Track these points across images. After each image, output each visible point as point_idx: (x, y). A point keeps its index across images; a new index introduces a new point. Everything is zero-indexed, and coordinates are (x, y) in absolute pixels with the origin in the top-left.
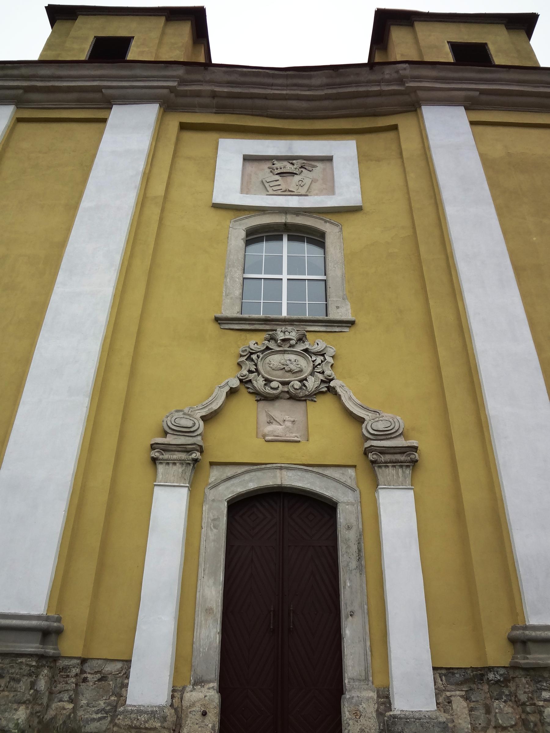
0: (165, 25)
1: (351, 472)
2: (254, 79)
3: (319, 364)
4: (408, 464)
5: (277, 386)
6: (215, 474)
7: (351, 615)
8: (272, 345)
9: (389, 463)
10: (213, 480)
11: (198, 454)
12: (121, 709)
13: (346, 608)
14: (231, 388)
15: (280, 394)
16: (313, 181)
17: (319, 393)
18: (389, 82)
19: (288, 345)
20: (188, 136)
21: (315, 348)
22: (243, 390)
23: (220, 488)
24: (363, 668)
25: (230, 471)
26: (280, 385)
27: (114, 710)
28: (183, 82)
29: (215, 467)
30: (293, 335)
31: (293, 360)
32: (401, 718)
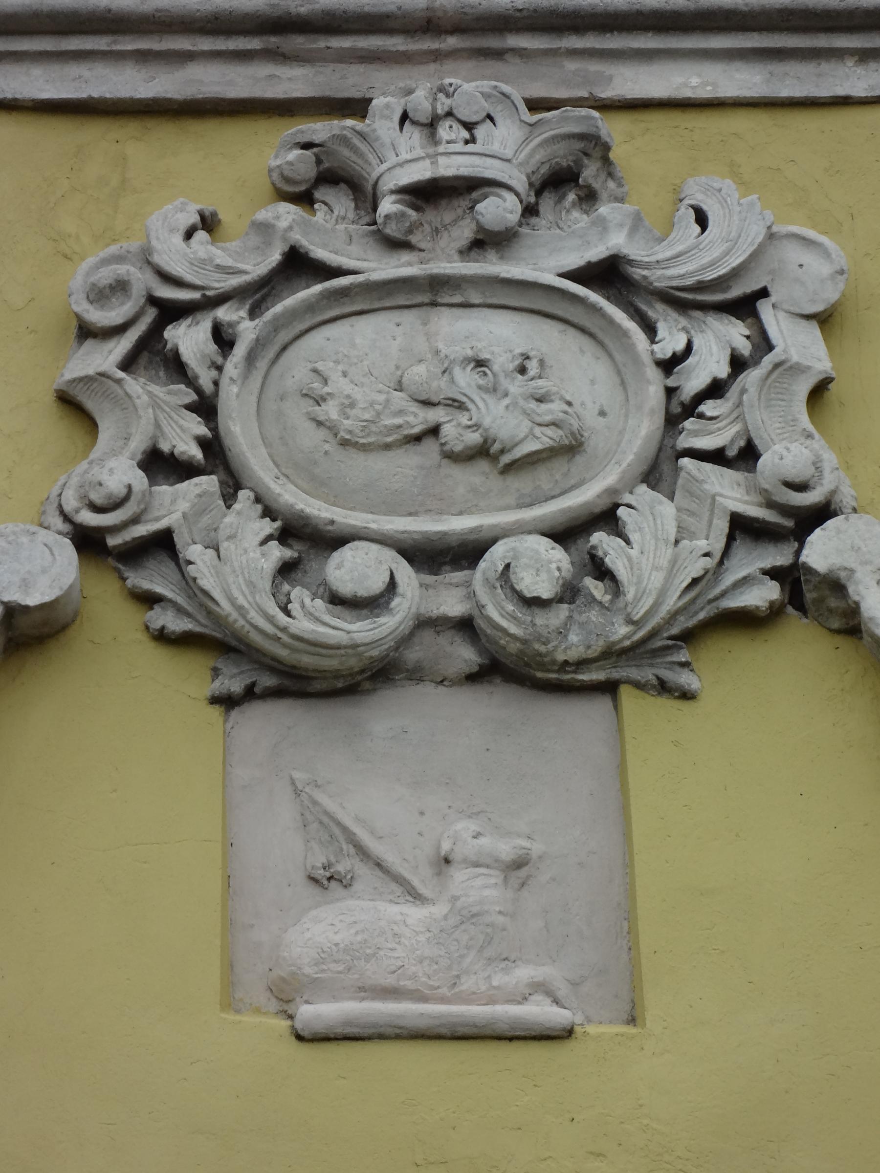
3: (715, 389)
5: (376, 584)
15: (405, 640)
21: (678, 256)
26: (405, 573)
30: (507, 150)
31: (502, 362)
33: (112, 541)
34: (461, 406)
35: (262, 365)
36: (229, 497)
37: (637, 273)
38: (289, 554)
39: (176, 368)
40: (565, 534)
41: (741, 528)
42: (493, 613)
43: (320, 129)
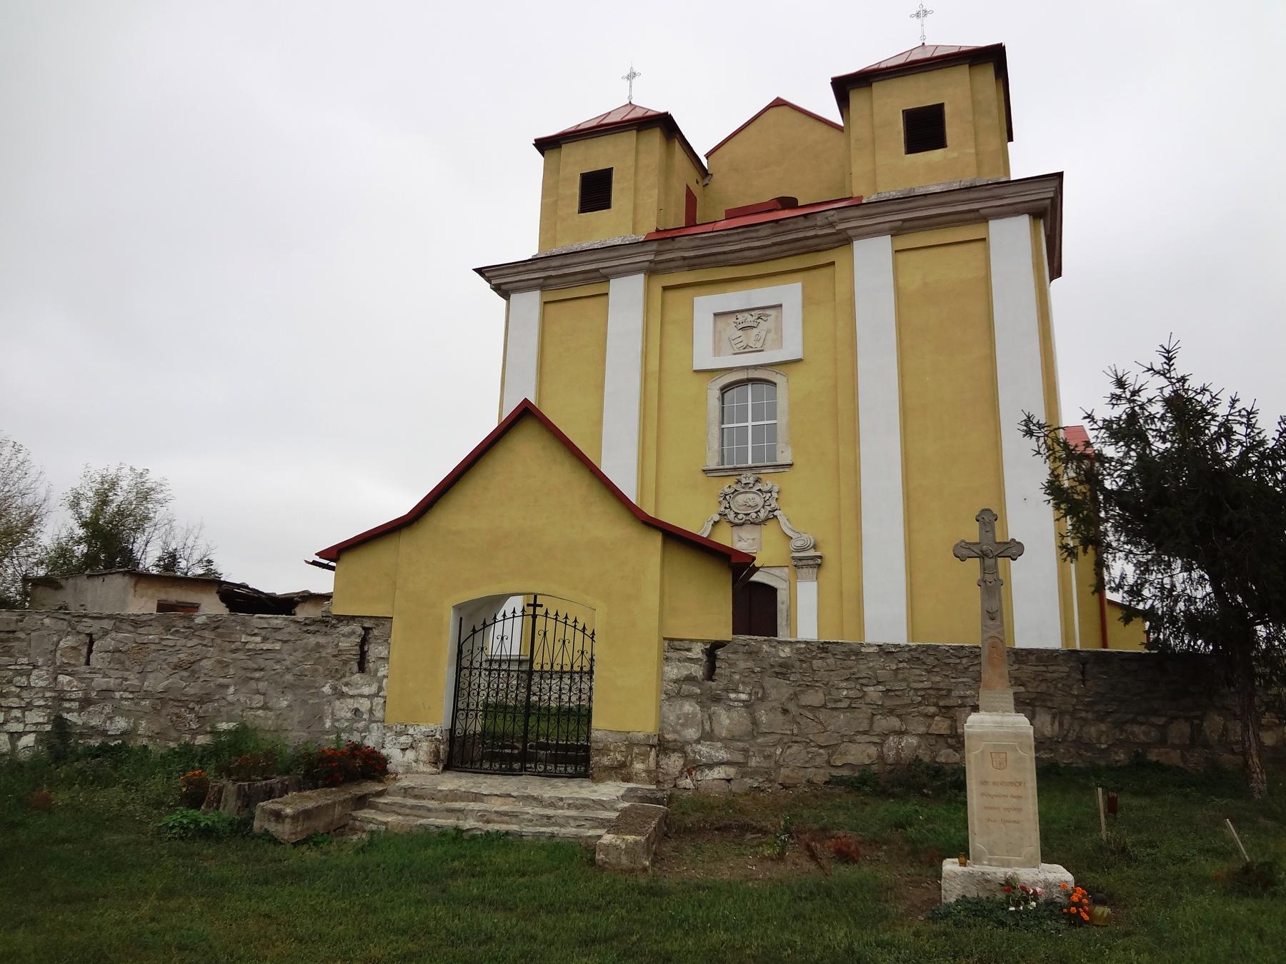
0: (637, 139)
1: (786, 570)
2: (713, 241)
8: (738, 487)
16: (768, 331)
17: (767, 519)
18: (822, 227)
20: (671, 295)
28: (658, 253)
30: (751, 480)
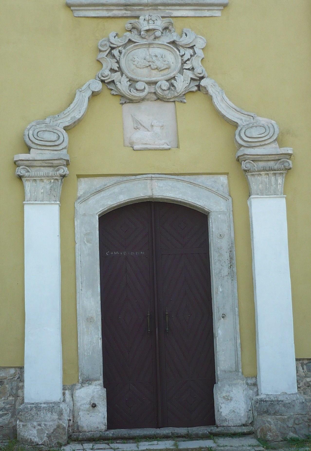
1: (223, 179)
3: (188, 60)
4: (281, 172)
5: (143, 88)
6: (83, 186)
7: (223, 317)
9: (262, 171)
10: (81, 193)
11: (66, 169)
12: (22, 407)
13: (219, 311)
14: (93, 92)
15: (146, 95)
19: (153, 37)
21: (184, 41)
22: (107, 92)
23: (89, 202)
24: (234, 362)
25: (98, 183)
26: (147, 86)
27: (13, 408)
29: (82, 179)
30: (160, 24)
31: (159, 56)
32: (266, 401)
33: (106, 81)
34: (154, 62)
35: (126, 56)
36: (122, 75)
37: (177, 43)
38: (130, 83)
39: (114, 56)
40: (167, 81)
41: (192, 79)
42: (158, 91)
43: (133, 21)
